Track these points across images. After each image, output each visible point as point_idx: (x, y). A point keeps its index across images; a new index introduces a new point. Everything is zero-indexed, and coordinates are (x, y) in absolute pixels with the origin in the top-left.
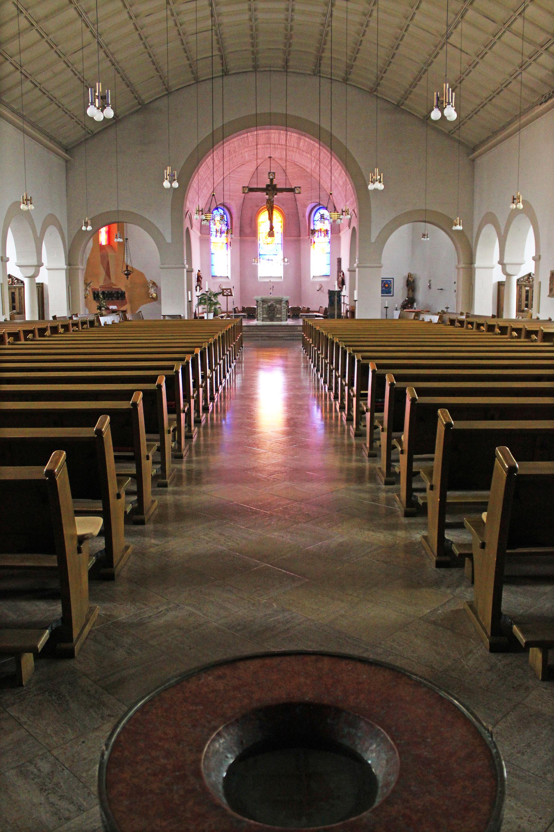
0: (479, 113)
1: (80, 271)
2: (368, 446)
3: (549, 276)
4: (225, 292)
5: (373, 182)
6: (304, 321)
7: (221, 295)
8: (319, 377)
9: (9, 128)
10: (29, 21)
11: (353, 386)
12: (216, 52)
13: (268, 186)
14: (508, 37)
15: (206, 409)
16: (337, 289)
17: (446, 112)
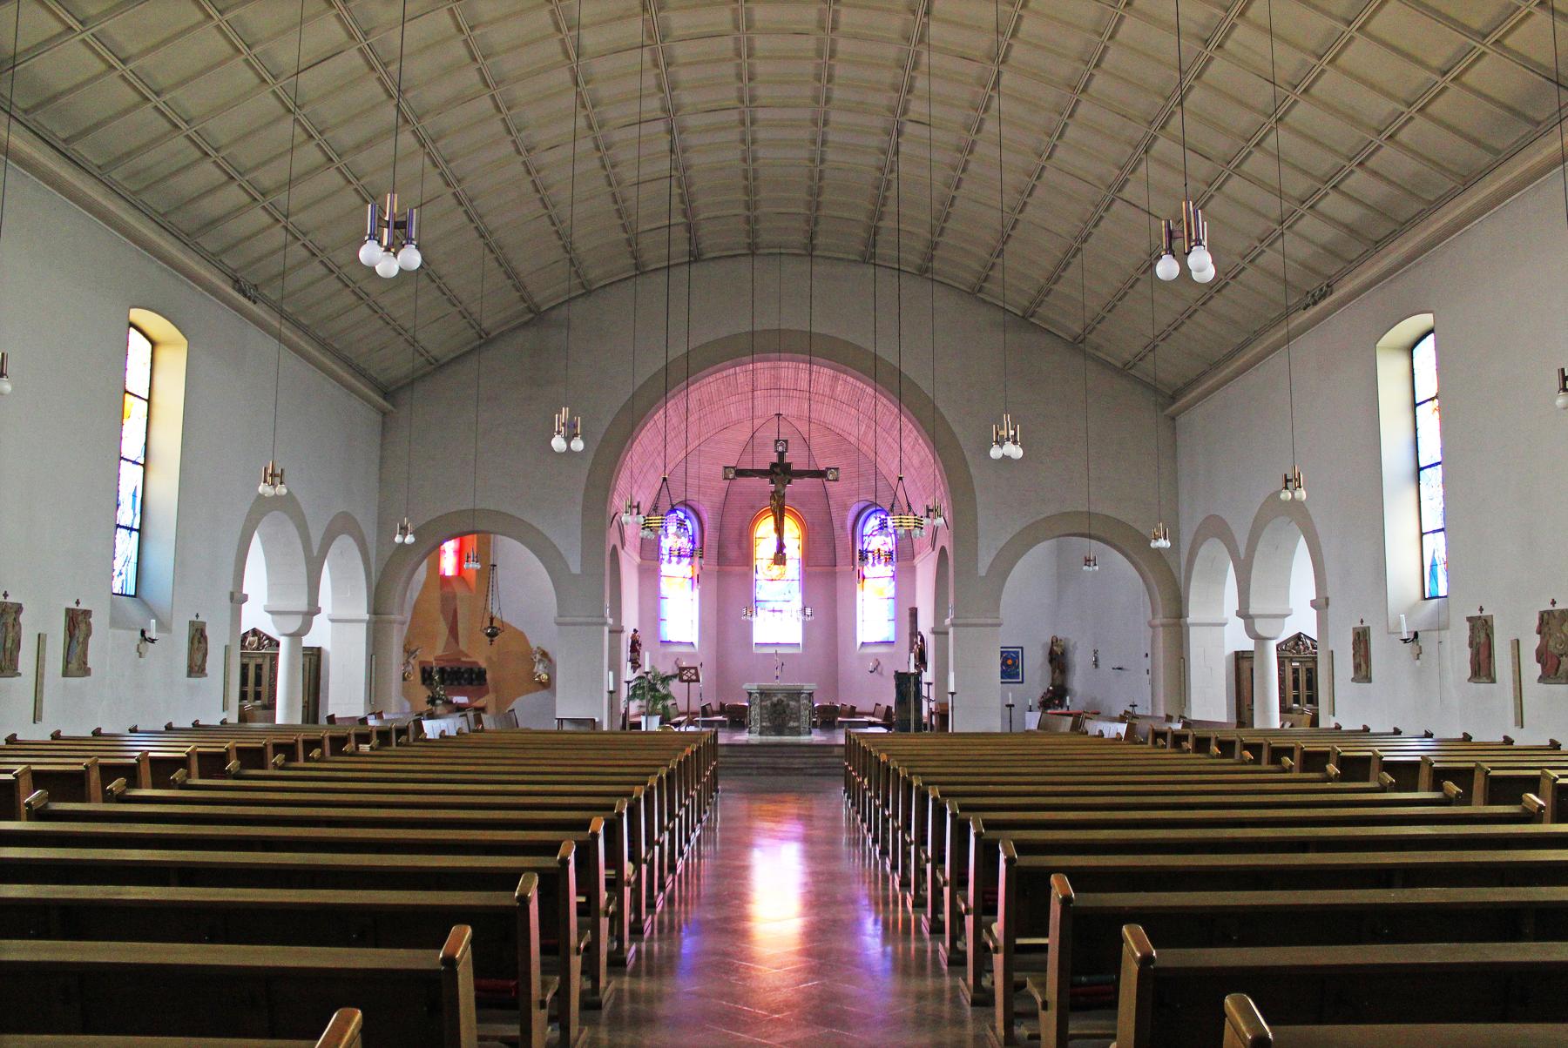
0: (1183, 329)
1: (396, 627)
3: (1351, 639)
4: (685, 674)
5: (1000, 443)
6: (848, 736)
7: (676, 681)
8: (888, 869)
9: (23, 192)
10: (325, 153)
12: (678, 219)
13: (773, 465)
14: (1235, 185)
16: (913, 670)
17: (1192, 261)
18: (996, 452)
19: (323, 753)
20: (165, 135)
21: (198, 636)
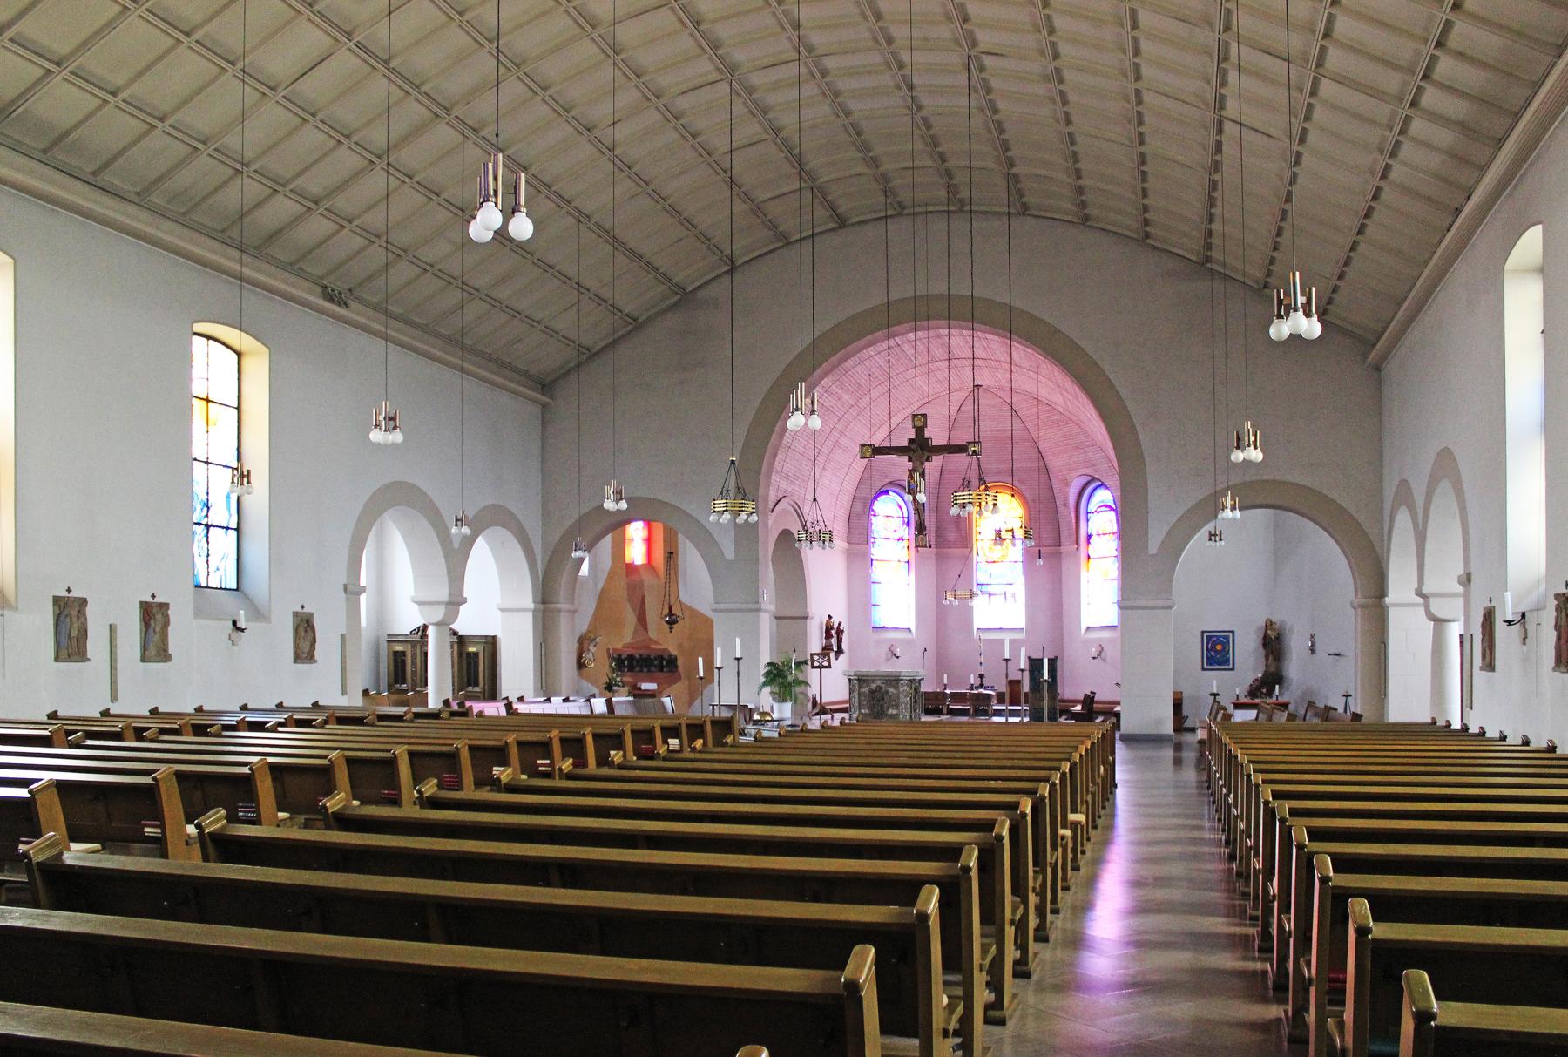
13: (911, 441)
19: (705, 744)
20: (184, 160)
21: (304, 626)
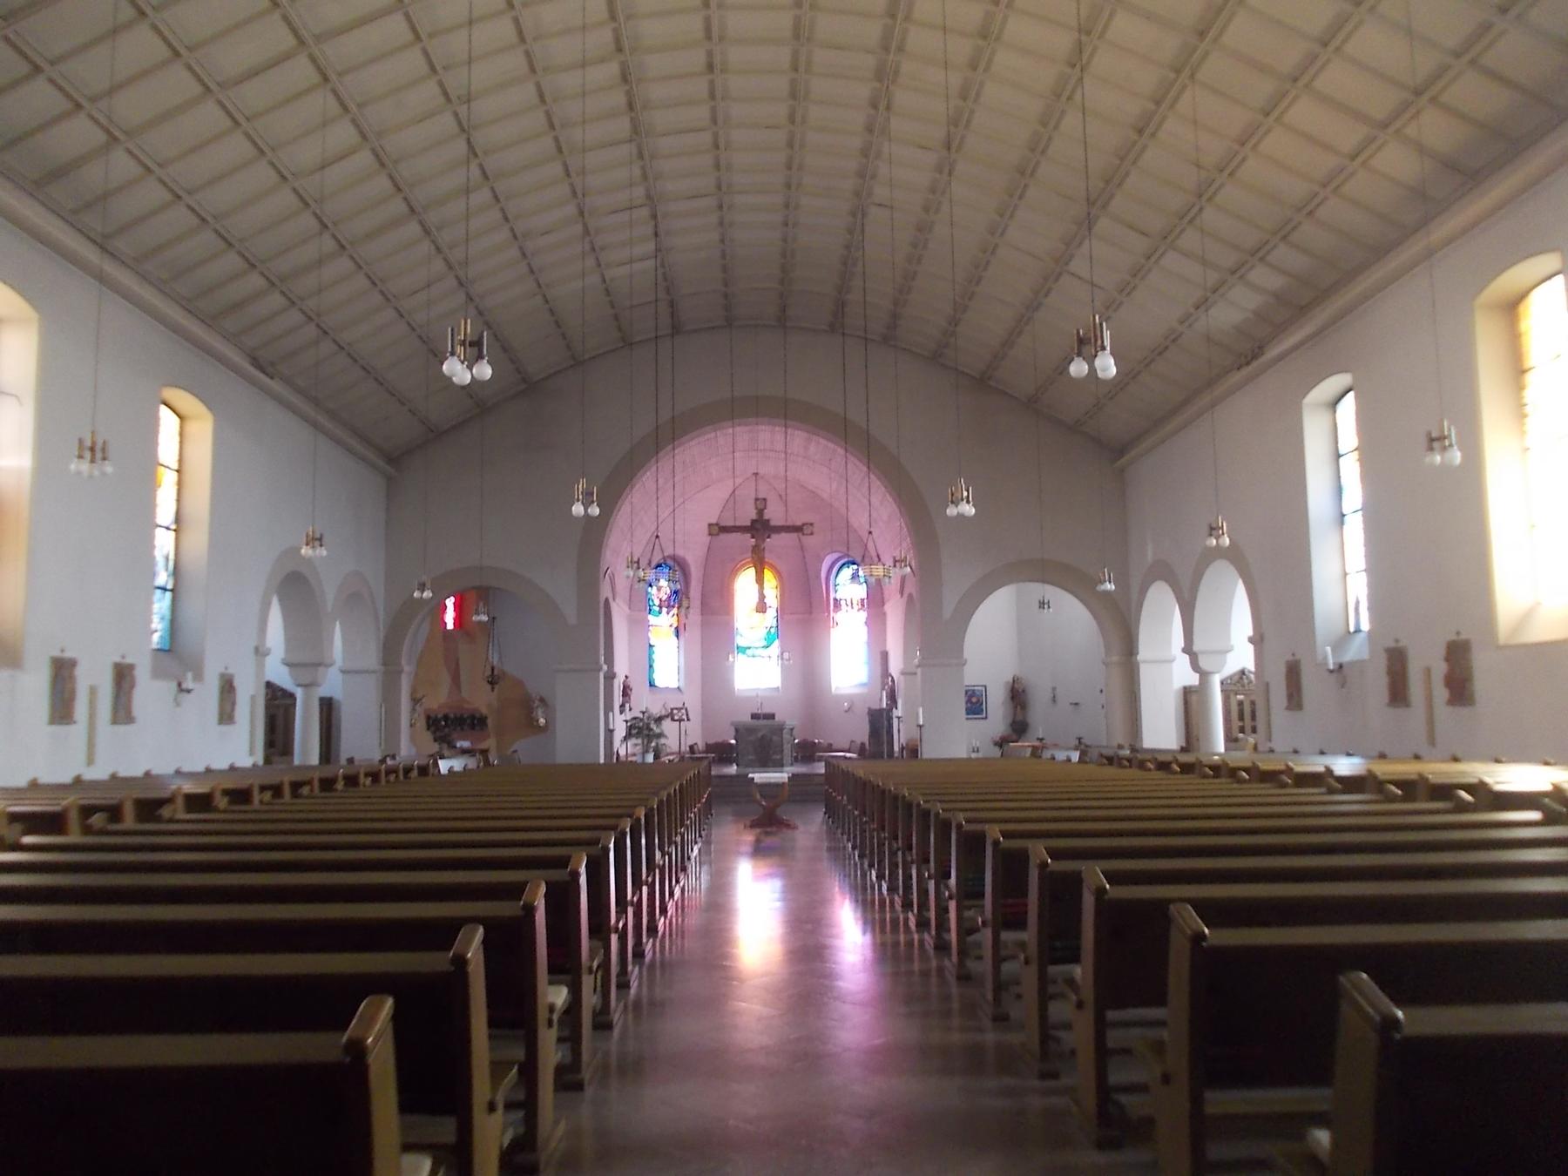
2: (990, 997)
5: (955, 503)
11: (949, 877)
13: (753, 522)
15: (653, 930)
17: (1098, 362)
18: (952, 511)
